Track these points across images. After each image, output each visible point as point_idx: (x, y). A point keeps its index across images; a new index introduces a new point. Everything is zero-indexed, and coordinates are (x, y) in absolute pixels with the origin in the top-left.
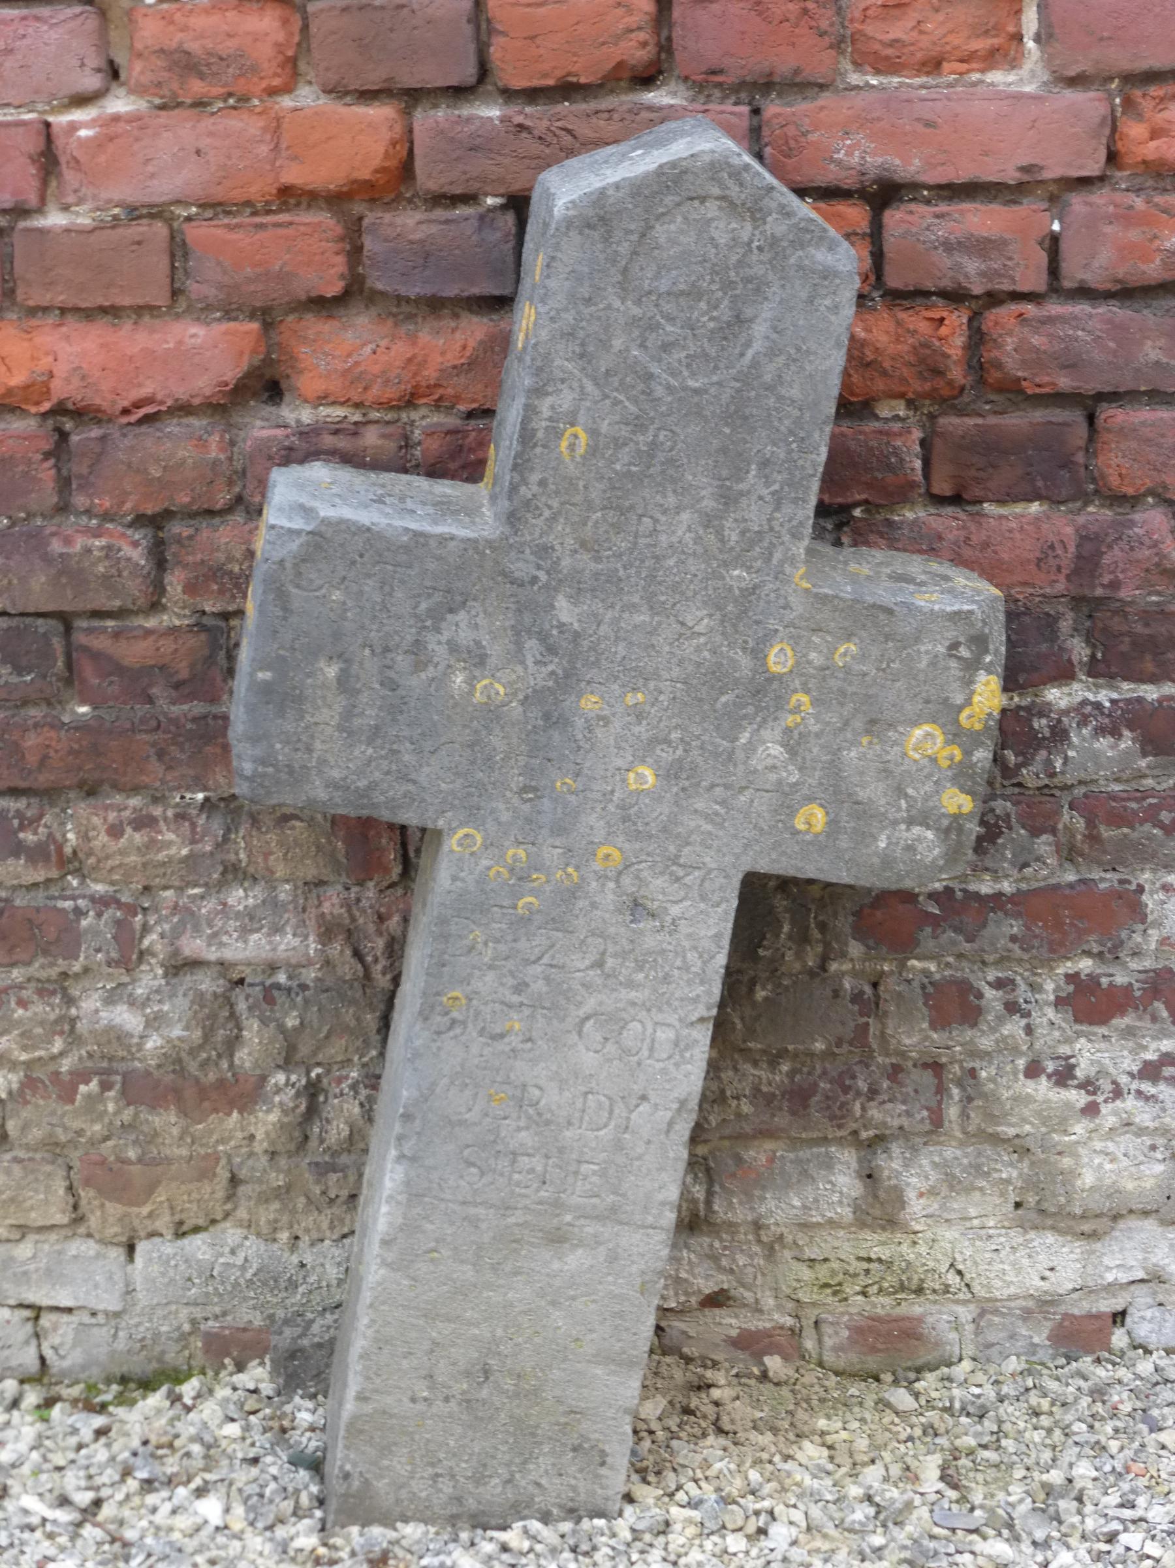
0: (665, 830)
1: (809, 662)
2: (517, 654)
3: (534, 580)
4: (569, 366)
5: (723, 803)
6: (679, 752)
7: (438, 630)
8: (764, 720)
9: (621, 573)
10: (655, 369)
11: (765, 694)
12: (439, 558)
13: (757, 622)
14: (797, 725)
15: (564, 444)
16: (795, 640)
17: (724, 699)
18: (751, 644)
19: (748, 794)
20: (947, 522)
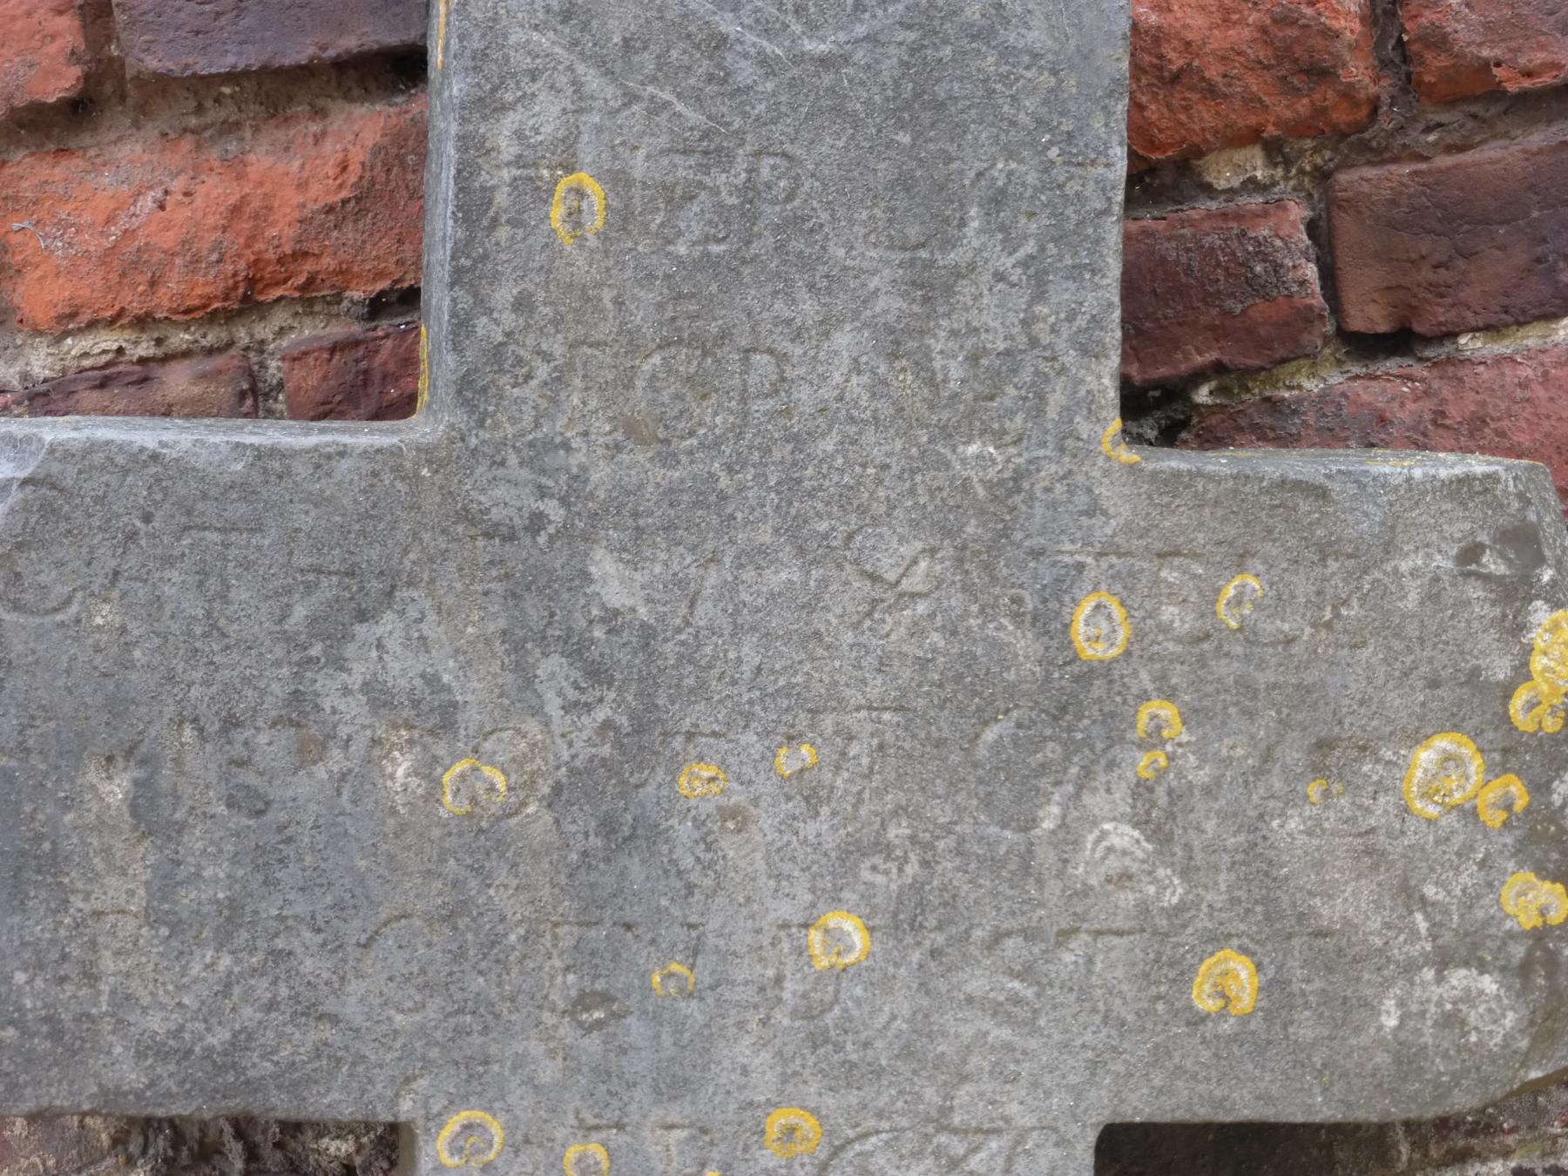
0: (907, 1052)
1: (1165, 629)
2: (522, 694)
3: (537, 522)
4: (543, 40)
5: (1026, 973)
6: (912, 868)
7: (340, 664)
8: (1087, 772)
9: (724, 482)
10: (728, 25)
11: (1076, 712)
12: (319, 501)
13: (1037, 554)
14: (1161, 774)
15: (557, 212)
16: (1125, 582)
17: (990, 735)
18: (1030, 604)
19: (1079, 943)
20: (1390, 386)
